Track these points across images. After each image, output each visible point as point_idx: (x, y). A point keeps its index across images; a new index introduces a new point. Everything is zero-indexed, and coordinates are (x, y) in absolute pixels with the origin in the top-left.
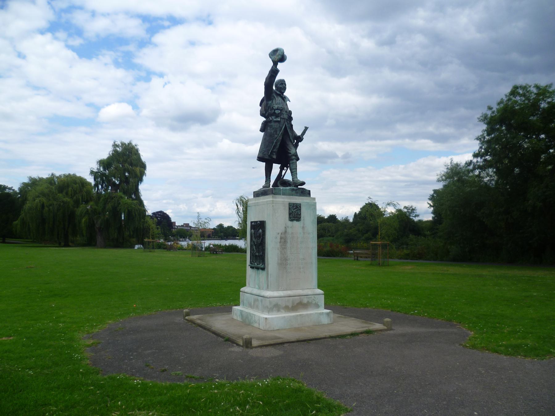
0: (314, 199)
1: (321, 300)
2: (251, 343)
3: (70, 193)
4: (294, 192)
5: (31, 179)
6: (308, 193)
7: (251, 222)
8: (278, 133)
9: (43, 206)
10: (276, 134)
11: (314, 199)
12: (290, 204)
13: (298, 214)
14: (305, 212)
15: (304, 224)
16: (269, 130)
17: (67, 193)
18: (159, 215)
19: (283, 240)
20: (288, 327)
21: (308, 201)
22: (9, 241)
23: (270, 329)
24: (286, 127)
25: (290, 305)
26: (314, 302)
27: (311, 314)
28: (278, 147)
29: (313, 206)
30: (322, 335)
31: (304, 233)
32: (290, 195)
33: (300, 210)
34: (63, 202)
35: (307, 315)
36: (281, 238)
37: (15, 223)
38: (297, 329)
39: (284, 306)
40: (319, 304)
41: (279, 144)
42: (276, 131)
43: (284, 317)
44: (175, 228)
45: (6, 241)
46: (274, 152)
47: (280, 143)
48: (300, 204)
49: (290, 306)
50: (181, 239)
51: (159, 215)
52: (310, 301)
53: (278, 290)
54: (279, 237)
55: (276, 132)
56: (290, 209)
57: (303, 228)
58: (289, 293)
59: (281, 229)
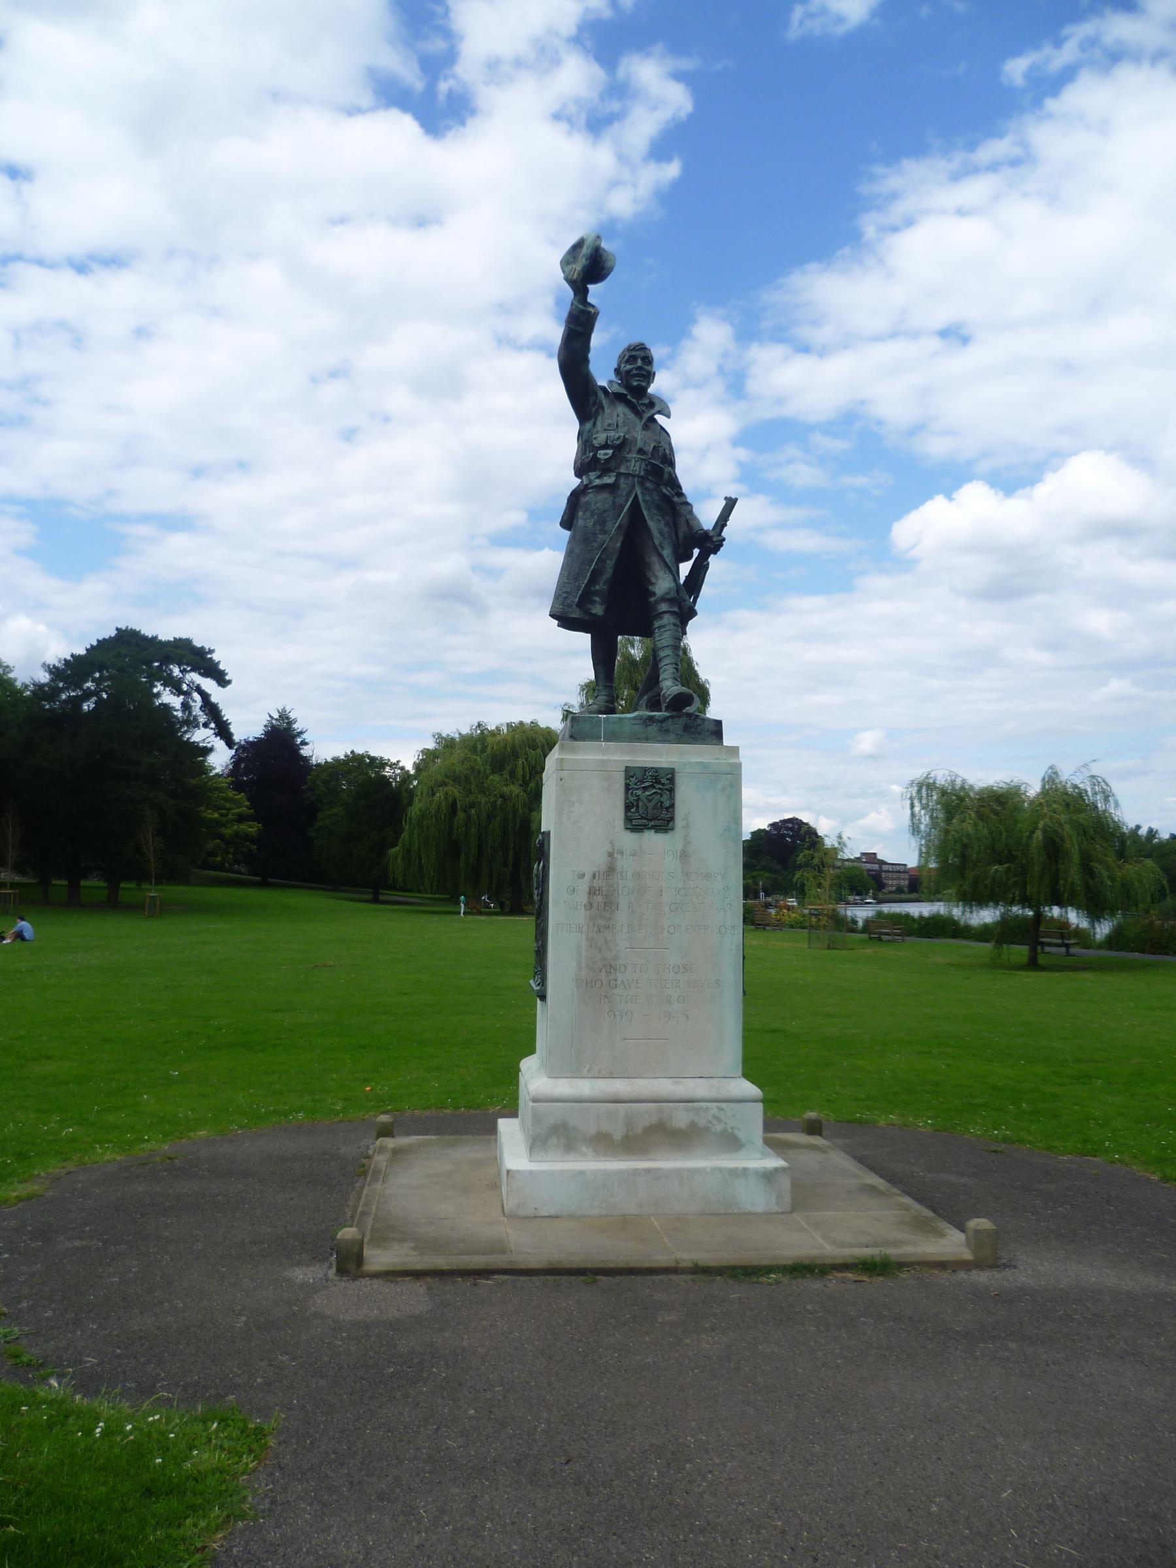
0: (734, 751)
2: (359, 1260)
3: (520, 772)
4: (653, 729)
6: (716, 730)
9: (453, 807)
10: (605, 532)
11: (734, 751)
12: (629, 772)
14: (689, 799)
15: (687, 843)
16: (583, 520)
17: (513, 774)
18: (788, 829)
19: (602, 898)
20: (595, 1212)
21: (705, 759)
22: (396, 898)
23: (521, 1212)
24: (635, 508)
26: (719, 1128)
27: (692, 1171)
28: (608, 573)
30: (662, 1259)
31: (687, 874)
33: (672, 791)
34: (502, 796)
35: (678, 1172)
36: (592, 892)
37: (393, 850)
38: (624, 1224)
39: (592, 1131)
40: (740, 1135)
41: (610, 564)
42: (602, 523)
43: (582, 1173)
44: (835, 867)
45: (381, 898)
46: (597, 593)
47: (632, 555)
48: (673, 769)
49: (618, 1136)
50: (851, 898)
51: (788, 829)
52: (702, 1123)
54: (583, 887)
56: (627, 787)
57: (684, 856)
58: (619, 1086)
59: (595, 860)
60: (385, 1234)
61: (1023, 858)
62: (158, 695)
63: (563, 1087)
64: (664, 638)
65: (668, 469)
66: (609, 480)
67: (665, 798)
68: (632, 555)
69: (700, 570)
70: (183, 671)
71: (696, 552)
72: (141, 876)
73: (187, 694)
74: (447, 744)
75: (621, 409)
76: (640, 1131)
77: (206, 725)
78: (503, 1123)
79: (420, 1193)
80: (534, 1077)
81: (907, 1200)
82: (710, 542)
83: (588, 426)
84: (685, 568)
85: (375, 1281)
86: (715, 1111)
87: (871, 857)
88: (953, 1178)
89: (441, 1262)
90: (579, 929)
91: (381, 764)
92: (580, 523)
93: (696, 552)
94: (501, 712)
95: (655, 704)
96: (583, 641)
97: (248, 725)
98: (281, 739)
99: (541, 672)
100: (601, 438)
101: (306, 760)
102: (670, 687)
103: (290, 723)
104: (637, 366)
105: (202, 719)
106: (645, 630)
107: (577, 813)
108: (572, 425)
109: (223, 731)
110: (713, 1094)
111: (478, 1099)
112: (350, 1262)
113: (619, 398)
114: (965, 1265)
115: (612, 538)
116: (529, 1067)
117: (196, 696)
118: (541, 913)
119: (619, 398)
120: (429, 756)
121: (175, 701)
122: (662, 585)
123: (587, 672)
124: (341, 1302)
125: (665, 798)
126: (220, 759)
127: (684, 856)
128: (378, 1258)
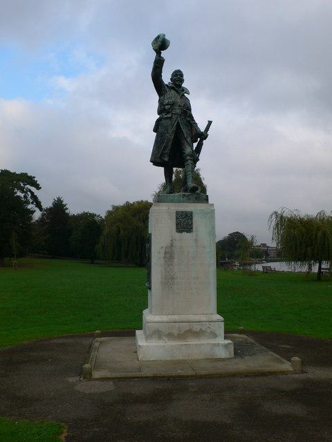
1: (220, 329)
2: (91, 375)
5: (114, 207)
7: (191, 213)
8: (169, 131)
11: (212, 205)
13: (188, 224)
14: (197, 221)
19: (169, 255)
24: (178, 124)
25: (176, 332)
29: (211, 214)
32: (179, 202)
33: (192, 219)
36: (166, 253)
41: (170, 144)
47: (177, 141)
52: (204, 329)
53: (161, 314)
55: (167, 130)
58: (176, 317)
60: (97, 367)
61: (306, 237)
62: (16, 193)
63: (157, 318)
64: (189, 168)
65: (189, 112)
66: (169, 116)
67: (189, 221)
68: (177, 141)
69: (200, 145)
70: (25, 185)
71: (199, 139)
72: (12, 256)
73: (26, 192)
74: (116, 209)
75: (173, 92)
76: (183, 332)
77: (32, 203)
78: (138, 332)
79: (110, 354)
80: (149, 316)
81: (272, 353)
82: (203, 136)
83: (162, 98)
84: (195, 145)
85: (96, 382)
86: (208, 325)
87: (264, 245)
88: (288, 347)
89: (118, 375)
90: (162, 266)
91: (93, 215)
92: (160, 130)
93: (199, 139)
94: (134, 197)
95: (186, 191)
96: (161, 170)
97: (47, 203)
98: (59, 206)
99: (149, 181)
100: (166, 102)
101: (68, 214)
102: (191, 184)
103: (62, 202)
104: (178, 77)
105: (31, 201)
106: (182, 166)
107: (161, 228)
108: (157, 97)
109: (38, 205)
110: (207, 319)
111: (129, 328)
112: (88, 376)
113: (172, 88)
114: (292, 373)
115: (170, 135)
116: (145, 312)
117: (29, 193)
118: (149, 268)
119: (172, 88)
120: (110, 213)
121: (22, 195)
122: (188, 150)
123: (163, 180)
124: (83, 387)
125: (189, 221)
126: (37, 215)
127: (196, 240)
128: (96, 375)
